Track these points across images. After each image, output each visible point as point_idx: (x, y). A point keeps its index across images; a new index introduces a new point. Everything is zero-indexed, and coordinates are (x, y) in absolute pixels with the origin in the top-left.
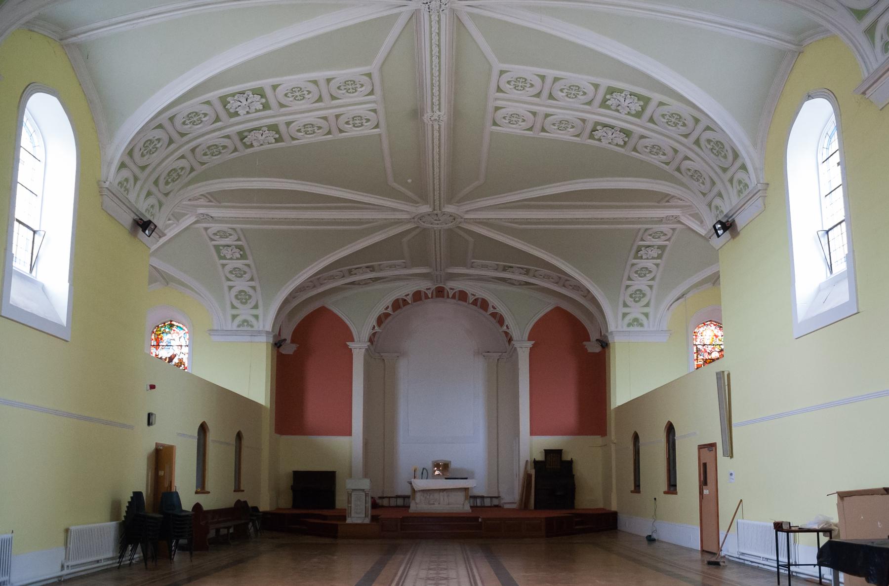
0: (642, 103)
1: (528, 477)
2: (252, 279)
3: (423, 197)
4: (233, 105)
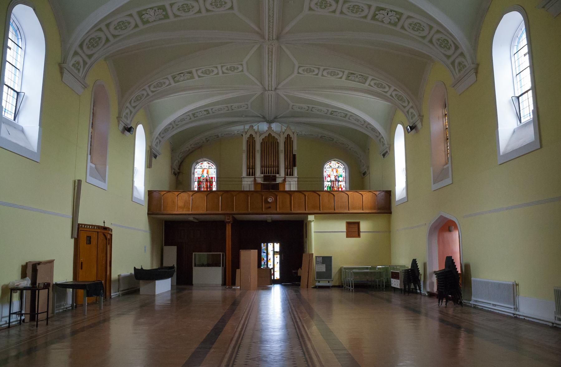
0: (398, 16)
4: (146, 17)
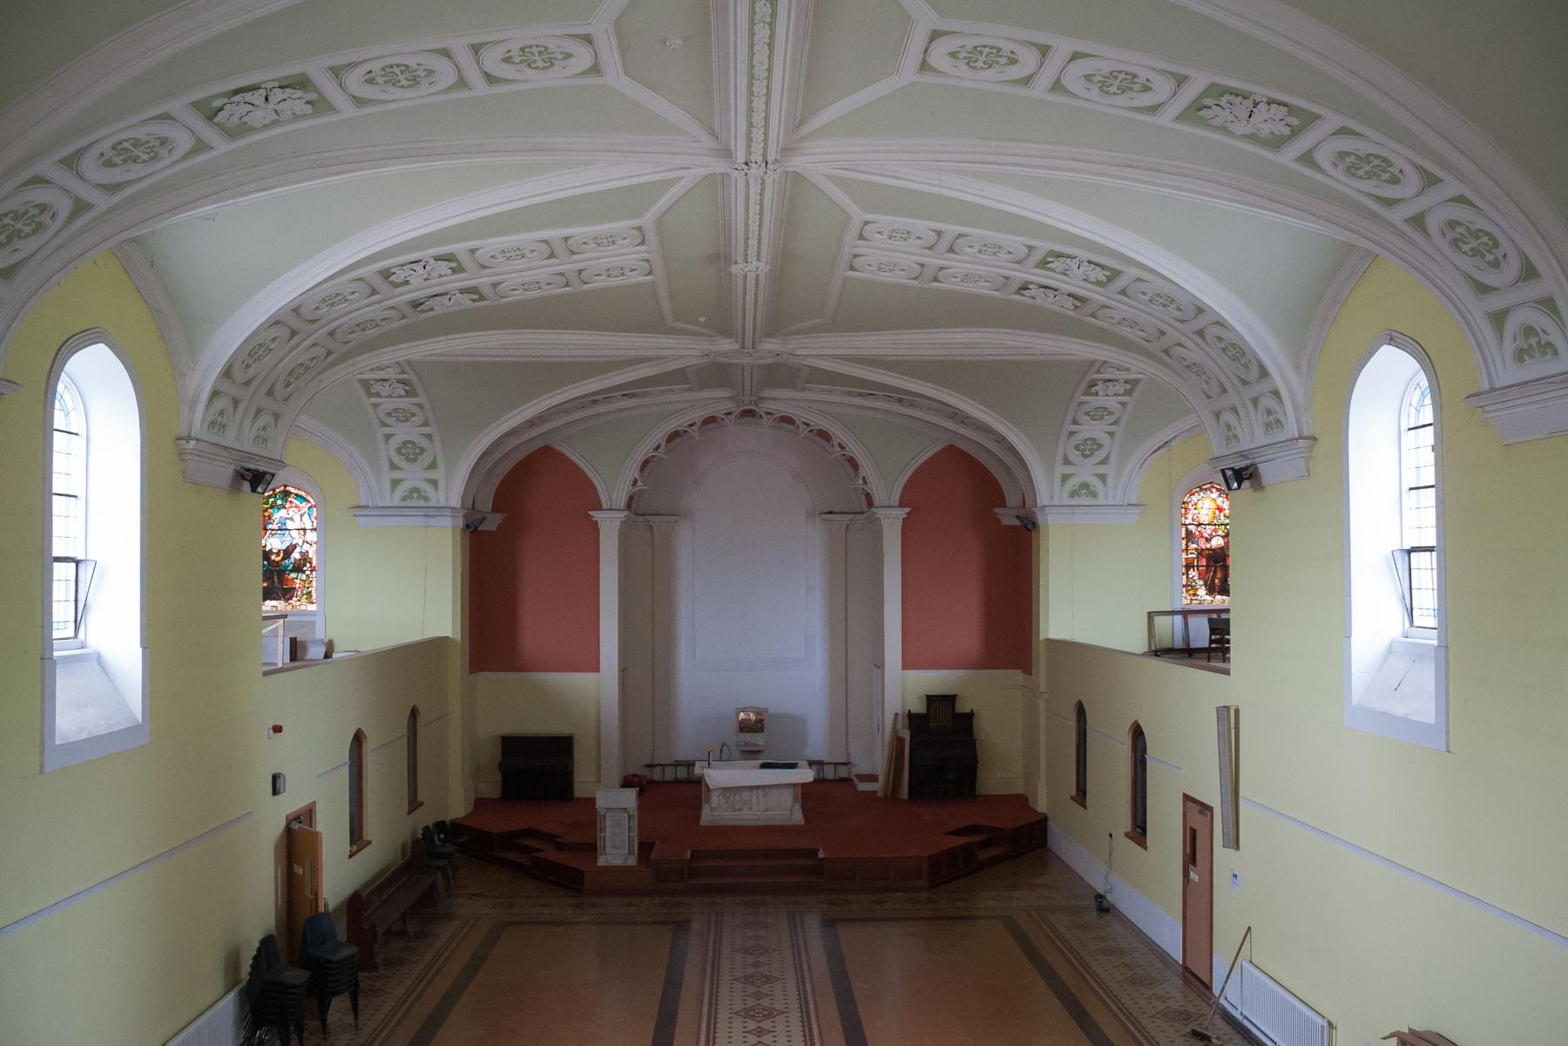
1: (899, 741)
2: (426, 424)
3: (726, 332)
